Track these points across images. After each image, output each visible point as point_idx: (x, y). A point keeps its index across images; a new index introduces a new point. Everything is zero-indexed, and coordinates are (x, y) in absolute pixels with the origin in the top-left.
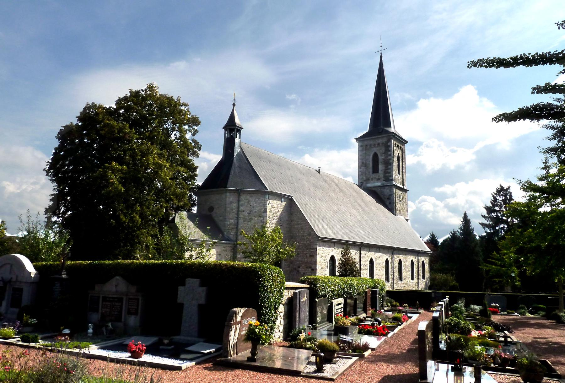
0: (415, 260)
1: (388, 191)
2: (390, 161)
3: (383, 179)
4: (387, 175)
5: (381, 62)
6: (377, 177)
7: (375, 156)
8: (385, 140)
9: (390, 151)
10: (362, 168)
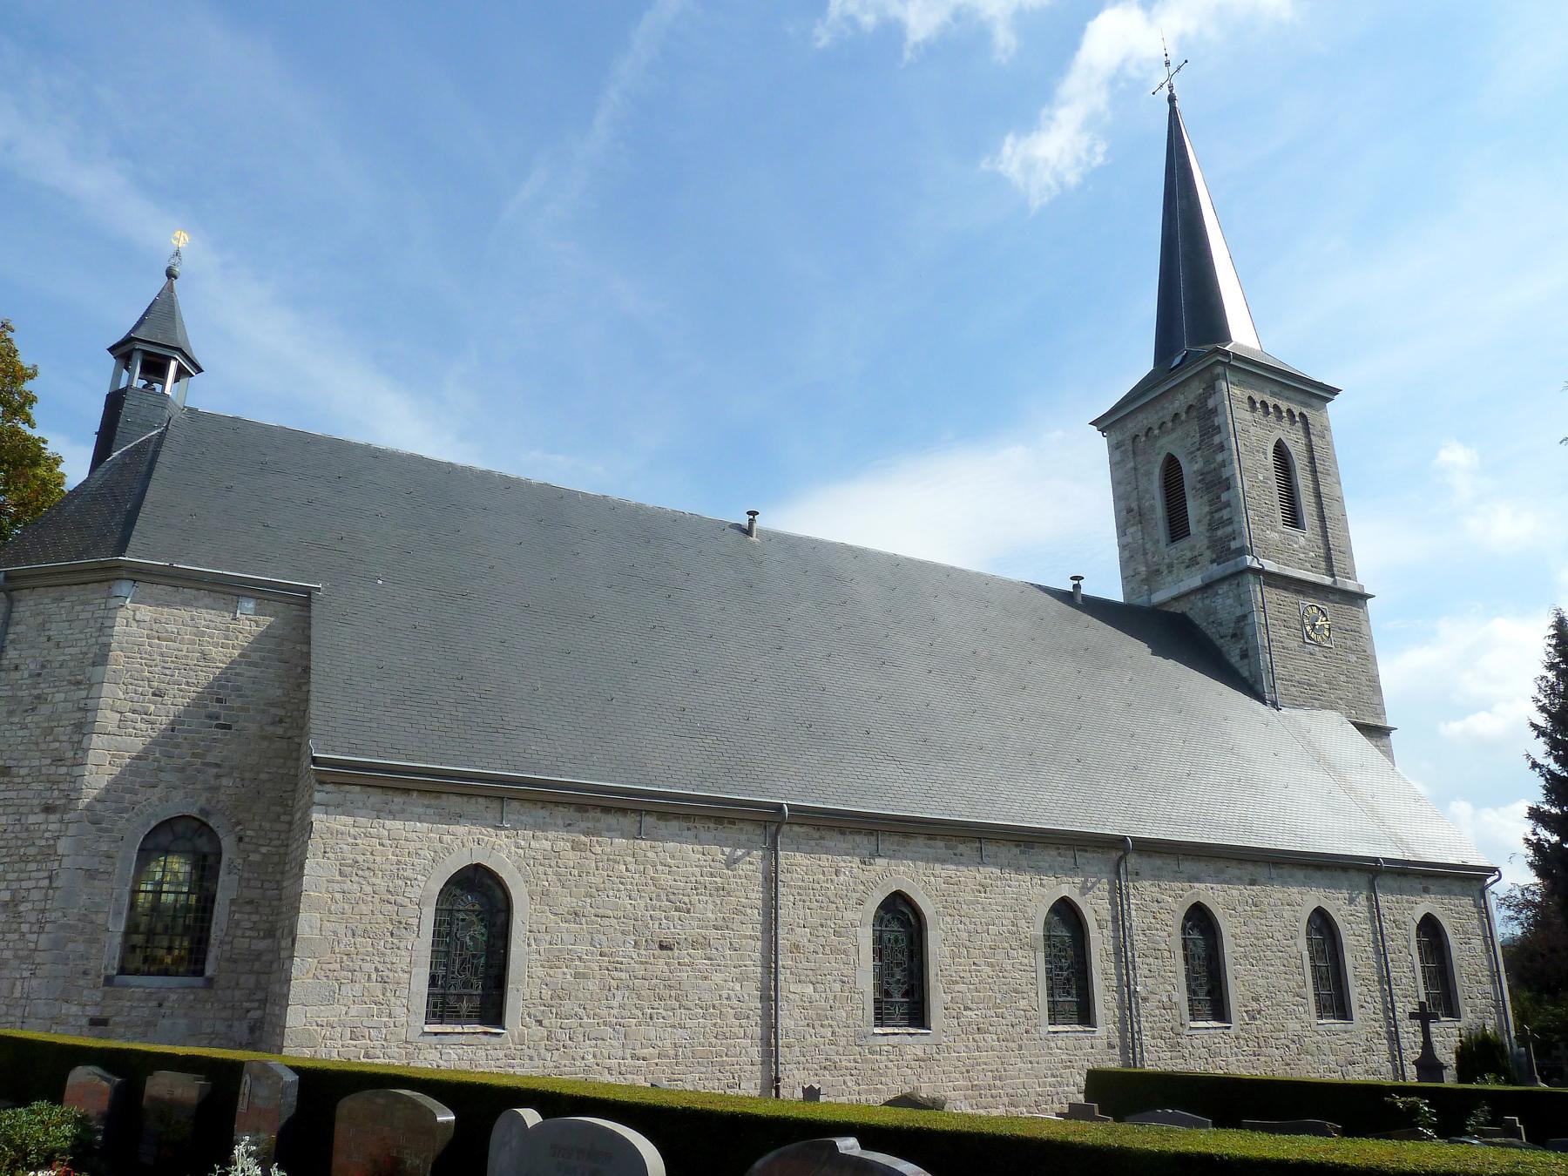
0: (1095, 908)
1: (1229, 601)
2: (1226, 473)
3: (1208, 555)
4: (1220, 533)
5: (1173, 113)
6: (1189, 555)
7: (1172, 468)
8: (1196, 389)
9: (1218, 429)
10: (1131, 530)
